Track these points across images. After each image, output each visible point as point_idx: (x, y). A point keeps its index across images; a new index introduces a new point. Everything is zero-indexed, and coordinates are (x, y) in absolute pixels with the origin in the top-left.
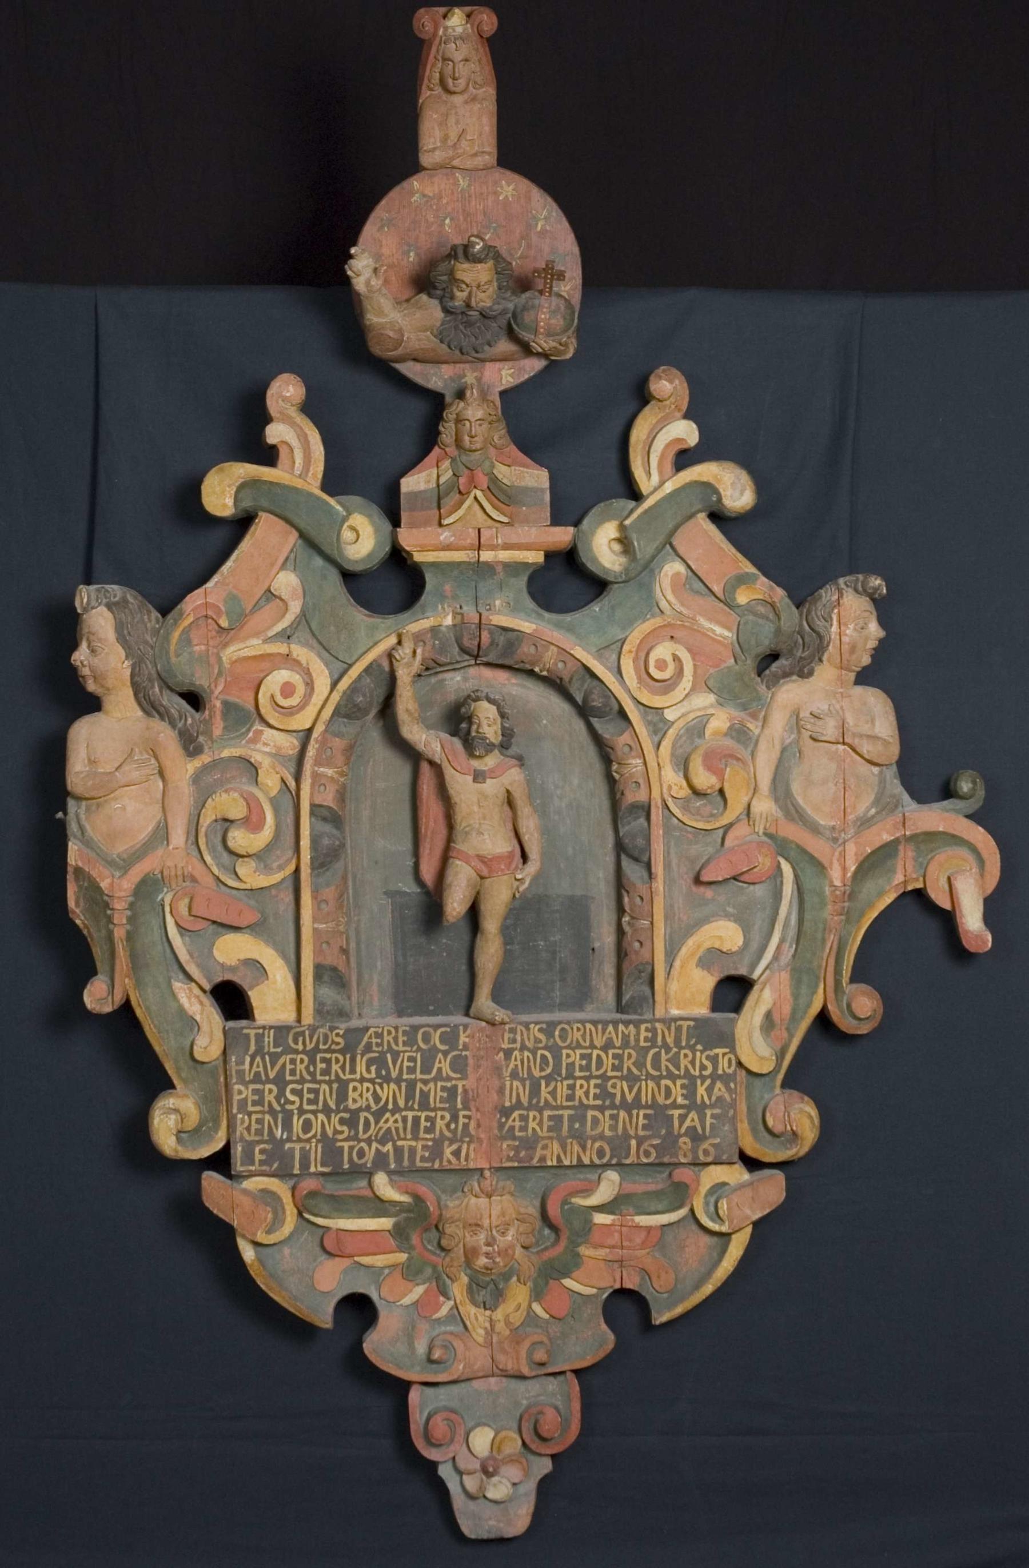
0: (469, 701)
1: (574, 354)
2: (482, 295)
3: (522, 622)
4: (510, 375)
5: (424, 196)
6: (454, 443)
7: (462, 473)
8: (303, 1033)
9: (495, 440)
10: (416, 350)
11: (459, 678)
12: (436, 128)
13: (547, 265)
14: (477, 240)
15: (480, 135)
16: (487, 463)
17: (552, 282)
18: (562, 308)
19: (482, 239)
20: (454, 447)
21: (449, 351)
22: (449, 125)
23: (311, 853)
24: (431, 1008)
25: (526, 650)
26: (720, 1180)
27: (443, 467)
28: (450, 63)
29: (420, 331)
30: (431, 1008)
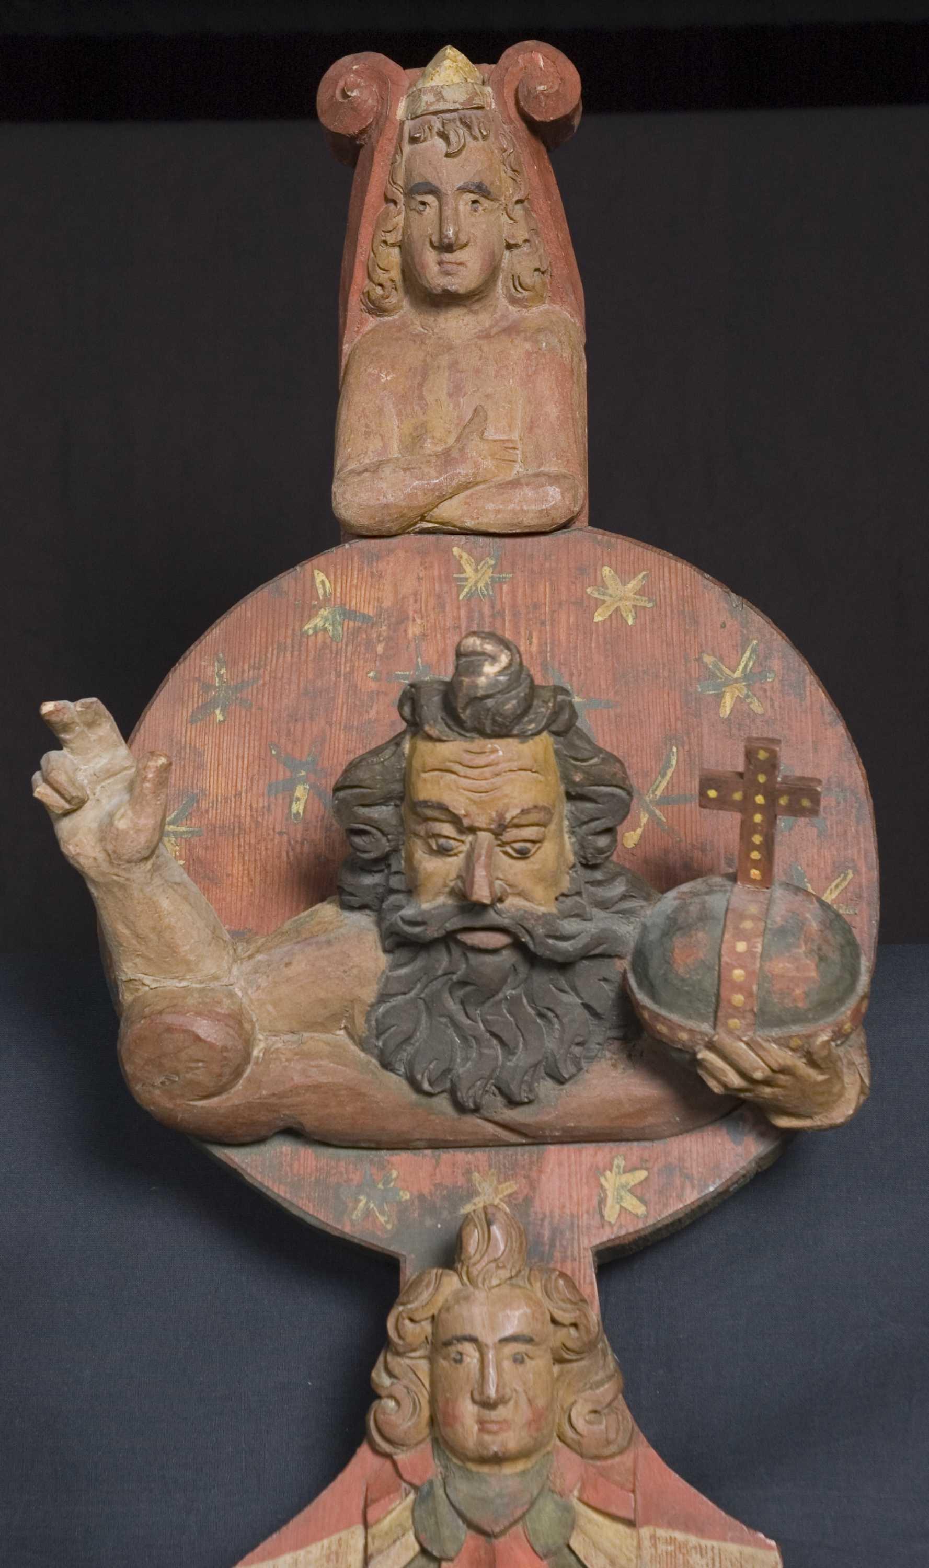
1: (860, 1111)
2: (515, 869)
4: (632, 1191)
5: (348, 614)
6: (425, 1431)
7: (450, 1550)
9: (580, 1424)
10: (295, 1090)
12: (390, 408)
13: (750, 755)
14: (489, 648)
15: (531, 428)
16: (548, 1511)
17: (771, 821)
18: (814, 925)
19: (505, 644)
20: (427, 1446)
21: (414, 1097)
22: (430, 398)
27: (386, 1524)
28: (430, 199)
29: (312, 1026)
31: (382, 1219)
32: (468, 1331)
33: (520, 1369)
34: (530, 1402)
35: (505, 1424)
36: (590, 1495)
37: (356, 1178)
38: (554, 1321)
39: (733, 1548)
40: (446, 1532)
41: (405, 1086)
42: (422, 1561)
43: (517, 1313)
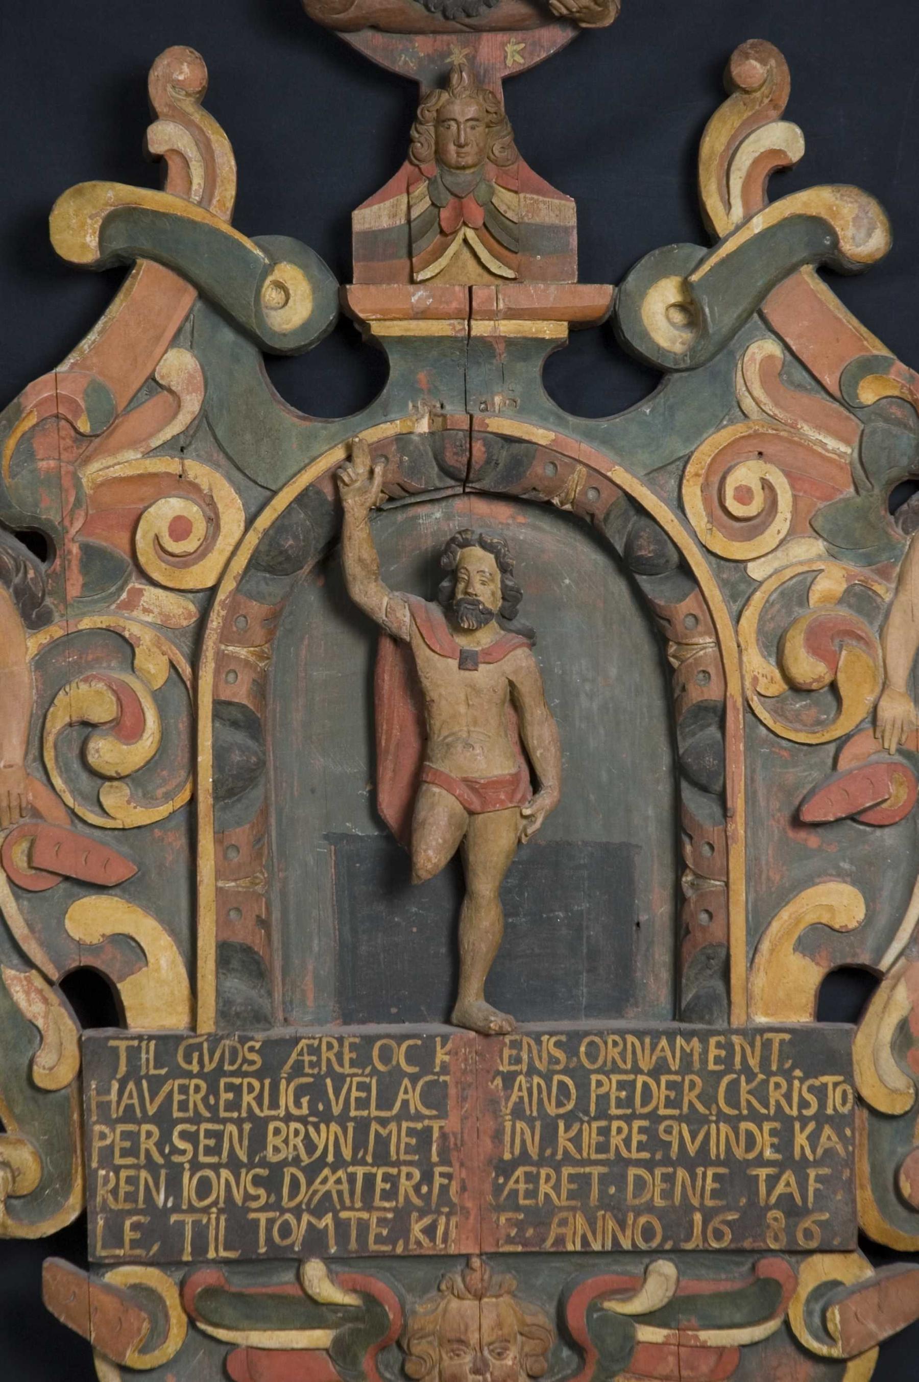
0: (453, 545)
3: (535, 430)
4: (518, 52)
6: (433, 155)
9: (496, 152)
11: (438, 515)
16: (483, 186)
20: (434, 162)
21: (427, 13)
24: (394, 1010)
25: (539, 470)
27: (416, 193)
30: (394, 1010)
31: (412, 65)
32: (452, 116)
33: (474, 131)
34: (477, 145)
35: (467, 154)
36: (500, 181)
37: (400, 47)
38: (487, 111)
39: (556, 201)
40: (442, 196)
41: (423, 9)
42: (432, 208)
43: (473, 109)
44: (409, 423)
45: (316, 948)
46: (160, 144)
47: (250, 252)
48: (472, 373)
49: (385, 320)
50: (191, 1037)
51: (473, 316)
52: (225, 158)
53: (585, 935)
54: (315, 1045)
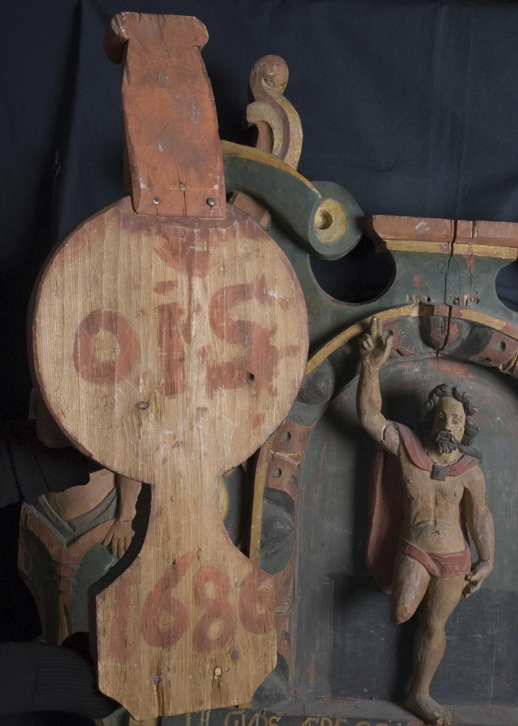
0: (434, 395)
3: (493, 319)
8: (239, 717)
11: (417, 370)
23: (262, 537)
24: (366, 690)
25: (493, 347)
26: (282, 473)
30: (366, 690)
44: (408, 310)
45: (317, 646)
46: (255, 117)
47: (309, 189)
48: (450, 278)
49: (396, 240)
50: (234, 710)
51: (456, 241)
52: (296, 129)
53: (495, 651)
54: (317, 722)
